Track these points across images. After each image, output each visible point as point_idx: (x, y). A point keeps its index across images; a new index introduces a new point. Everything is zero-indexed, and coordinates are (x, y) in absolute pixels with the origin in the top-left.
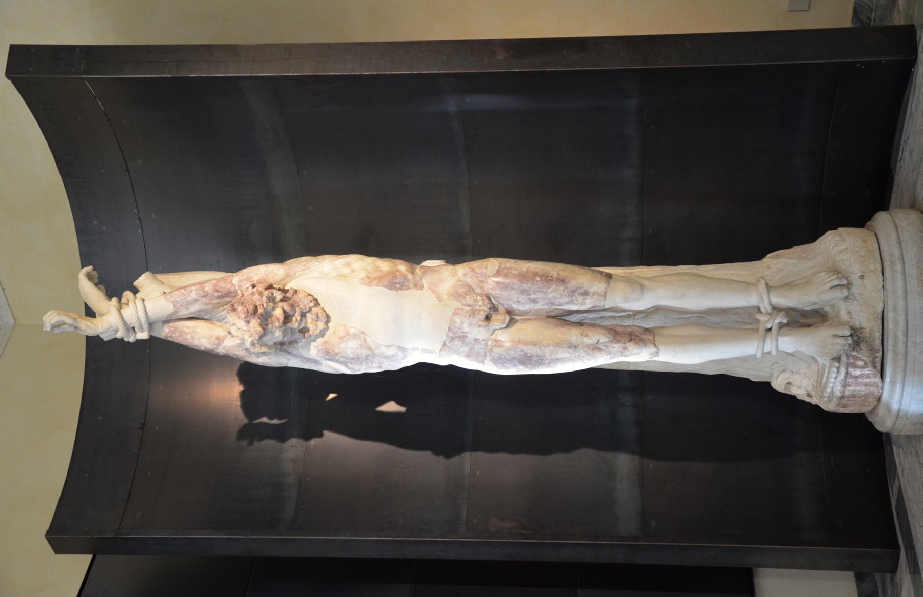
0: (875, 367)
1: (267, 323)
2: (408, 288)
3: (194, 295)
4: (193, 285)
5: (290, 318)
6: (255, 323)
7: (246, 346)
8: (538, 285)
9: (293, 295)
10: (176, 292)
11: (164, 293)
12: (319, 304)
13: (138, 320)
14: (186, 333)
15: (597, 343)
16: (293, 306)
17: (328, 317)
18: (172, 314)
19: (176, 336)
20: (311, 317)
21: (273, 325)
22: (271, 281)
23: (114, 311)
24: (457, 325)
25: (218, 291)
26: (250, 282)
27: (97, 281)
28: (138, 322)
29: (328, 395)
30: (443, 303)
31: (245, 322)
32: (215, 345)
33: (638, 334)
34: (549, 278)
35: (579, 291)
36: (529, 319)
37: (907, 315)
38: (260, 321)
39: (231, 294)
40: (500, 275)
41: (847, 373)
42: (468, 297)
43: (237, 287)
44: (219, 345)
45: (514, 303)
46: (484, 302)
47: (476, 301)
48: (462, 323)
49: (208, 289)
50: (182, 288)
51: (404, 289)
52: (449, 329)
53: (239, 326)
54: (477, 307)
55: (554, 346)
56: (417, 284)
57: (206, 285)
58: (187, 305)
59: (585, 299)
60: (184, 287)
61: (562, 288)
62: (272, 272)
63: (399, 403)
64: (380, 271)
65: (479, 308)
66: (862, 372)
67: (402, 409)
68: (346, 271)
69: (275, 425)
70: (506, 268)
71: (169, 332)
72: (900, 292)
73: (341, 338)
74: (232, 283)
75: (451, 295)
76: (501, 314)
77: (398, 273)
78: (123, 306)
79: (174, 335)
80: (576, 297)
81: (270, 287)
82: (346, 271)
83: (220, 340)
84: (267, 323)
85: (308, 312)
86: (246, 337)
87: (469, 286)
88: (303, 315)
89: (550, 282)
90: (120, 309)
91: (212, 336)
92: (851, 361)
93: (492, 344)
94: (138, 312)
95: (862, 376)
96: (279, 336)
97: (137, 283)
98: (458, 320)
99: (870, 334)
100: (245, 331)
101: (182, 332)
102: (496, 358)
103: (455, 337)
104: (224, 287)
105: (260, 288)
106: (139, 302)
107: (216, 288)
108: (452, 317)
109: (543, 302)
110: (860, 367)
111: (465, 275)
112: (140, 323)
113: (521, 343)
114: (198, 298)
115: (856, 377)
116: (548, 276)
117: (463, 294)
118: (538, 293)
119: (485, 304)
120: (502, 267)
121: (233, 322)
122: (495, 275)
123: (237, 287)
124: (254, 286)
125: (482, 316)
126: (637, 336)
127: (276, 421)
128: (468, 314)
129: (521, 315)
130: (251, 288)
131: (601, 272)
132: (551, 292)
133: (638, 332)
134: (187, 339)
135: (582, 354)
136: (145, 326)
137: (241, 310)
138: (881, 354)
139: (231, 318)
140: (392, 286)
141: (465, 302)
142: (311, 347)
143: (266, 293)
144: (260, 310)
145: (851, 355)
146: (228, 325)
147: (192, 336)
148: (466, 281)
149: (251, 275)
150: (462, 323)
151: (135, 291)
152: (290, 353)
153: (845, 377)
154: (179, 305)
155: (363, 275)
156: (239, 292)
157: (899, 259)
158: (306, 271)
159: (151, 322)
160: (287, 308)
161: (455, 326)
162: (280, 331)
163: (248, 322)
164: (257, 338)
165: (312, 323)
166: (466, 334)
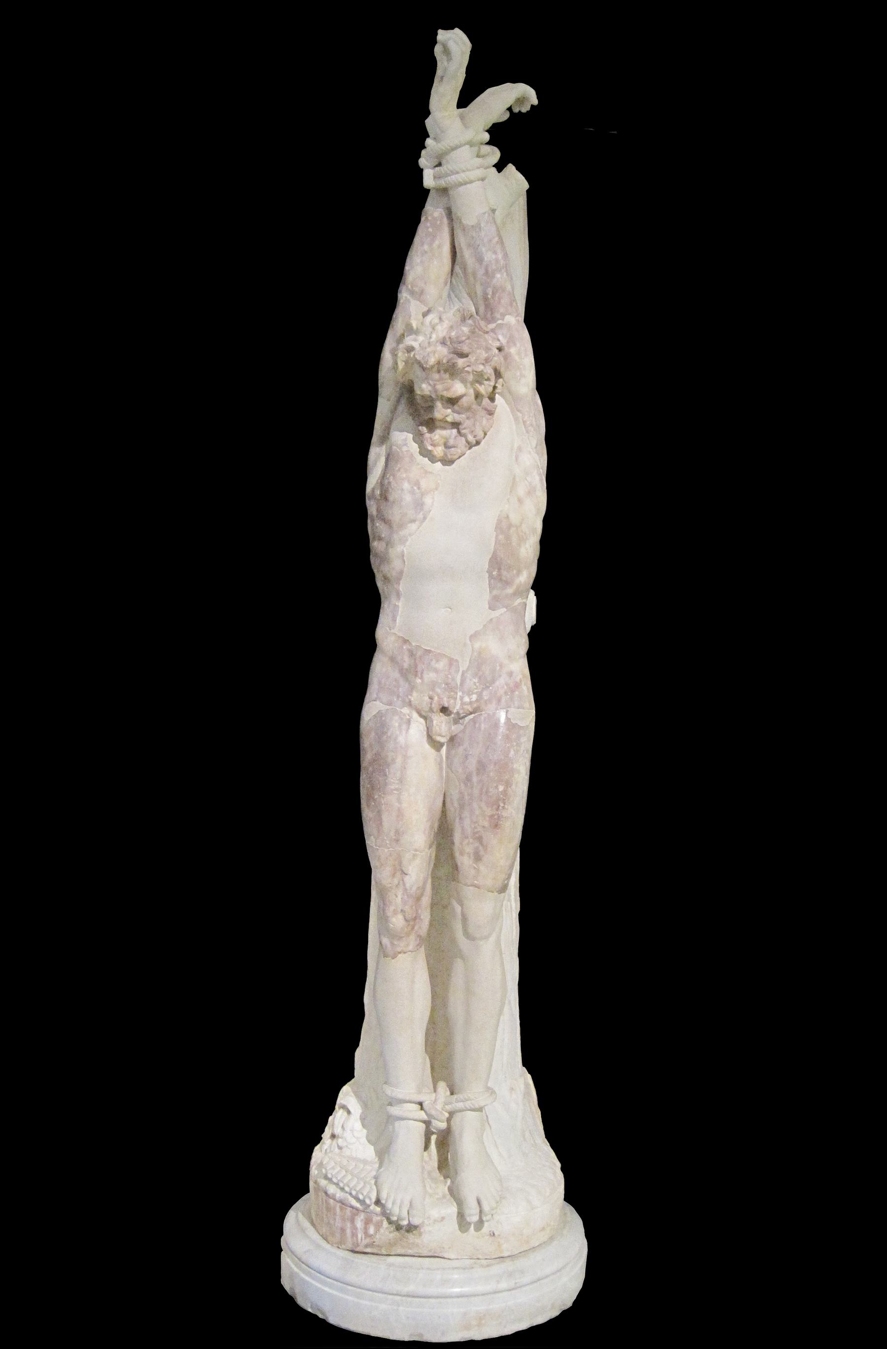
0: (366, 1246)
1: (442, 372)
2: (491, 588)
3: (489, 257)
4: (506, 255)
5: (451, 406)
6: (442, 353)
7: (407, 336)
9: (486, 409)
10: (494, 229)
11: (494, 211)
12: (470, 448)
13: (452, 172)
14: (431, 244)
15: (402, 871)
16: (468, 409)
17: (451, 462)
18: (461, 222)
19: (428, 228)
20: (450, 436)
21: (439, 381)
22: (507, 375)
23: (469, 135)
24: (433, 663)
25: (494, 293)
26: (508, 342)
27: (516, 110)
28: (449, 172)
30: (468, 642)
31: (444, 338)
32: (412, 287)
33: (416, 928)
34: (502, 805)
35: (481, 848)
36: (441, 769)
37: (437, 1297)
38: (444, 361)
39: (489, 313)
40: (508, 729)
42: (476, 680)
43: (500, 322)
44: (412, 293)
45: (465, 750)
46: (467, 704)
47: (470, 693)
48: (436, 671)
50: (500, 237)
53: (439, 328)
54: (460, 694)
56: (497, 601)
57: (505, 274)
58: (472, 246)
60: (501, 242)
62: (522, 376)
64: (519, 545)
65: (458, 697)
68: (521, 491)
70: (519, 737)
73: (417, 484)
74: (507, 314)
75: (480, 653)
76: (450, 728)
77: (515, 572)
78: (476, 149)
79: (428, 224)
81: (498, 374)
82: (521, 491)
83: (419, 295)
84: (442, 372)
85: (459, 432)
86: (421, 338)
87: (493, 681)
88: (456, 425)
90: (471, 144)
91: (425, 283)
93: (404, 715)
94: (464, 171)
95: (354, 1228)
96: (422, 390)
97: (511, 168)
99: (413, 1243)
100: (430, 338)
101: (434, 237)
102: (383, 719)
105: (497, 359)
106: (479, 173)
110: (366, 1229)
111: (510, 674)
112: (447, 175)
114: (484, 263)
115: (352, 1221)
116: (504, 804)
117: (481, 673)
119: (465, 707)
120: (521, 732)
121: (444, 317)
122: (508, 719)
123: (500, 322)
124: (500, 349)
126: (413, 928)
128: (450, 681)
129: (447, 758)
130: (498, 344)
131: (509, 877)
133: (420, 928)
134: (423, 244)
136: (442, 183)
137: (463, 331)
138: (385, 1253)
139: (451, 315)
140: (496, 563)
141: (468, 675)
142: (405, 433)
143: (489, 371)
144: (461, 362)
146: (441, 309)
147: (426, 252)
148: (500, 676)
149: (518, 345)
150: (436, 671)
151: (500, 167)
152: (398, 401)
154: (474, 235)
155: (514, 518)
156: (492, 326)
157: (516, 1283)
158: (523, 427)
159: (451, 192)
160: (464, 401)
161: (432, 660)
162: (430, 391)
163: (443, 343)
164: (418, 357)
165: (442, 437)
166: (420, 675)
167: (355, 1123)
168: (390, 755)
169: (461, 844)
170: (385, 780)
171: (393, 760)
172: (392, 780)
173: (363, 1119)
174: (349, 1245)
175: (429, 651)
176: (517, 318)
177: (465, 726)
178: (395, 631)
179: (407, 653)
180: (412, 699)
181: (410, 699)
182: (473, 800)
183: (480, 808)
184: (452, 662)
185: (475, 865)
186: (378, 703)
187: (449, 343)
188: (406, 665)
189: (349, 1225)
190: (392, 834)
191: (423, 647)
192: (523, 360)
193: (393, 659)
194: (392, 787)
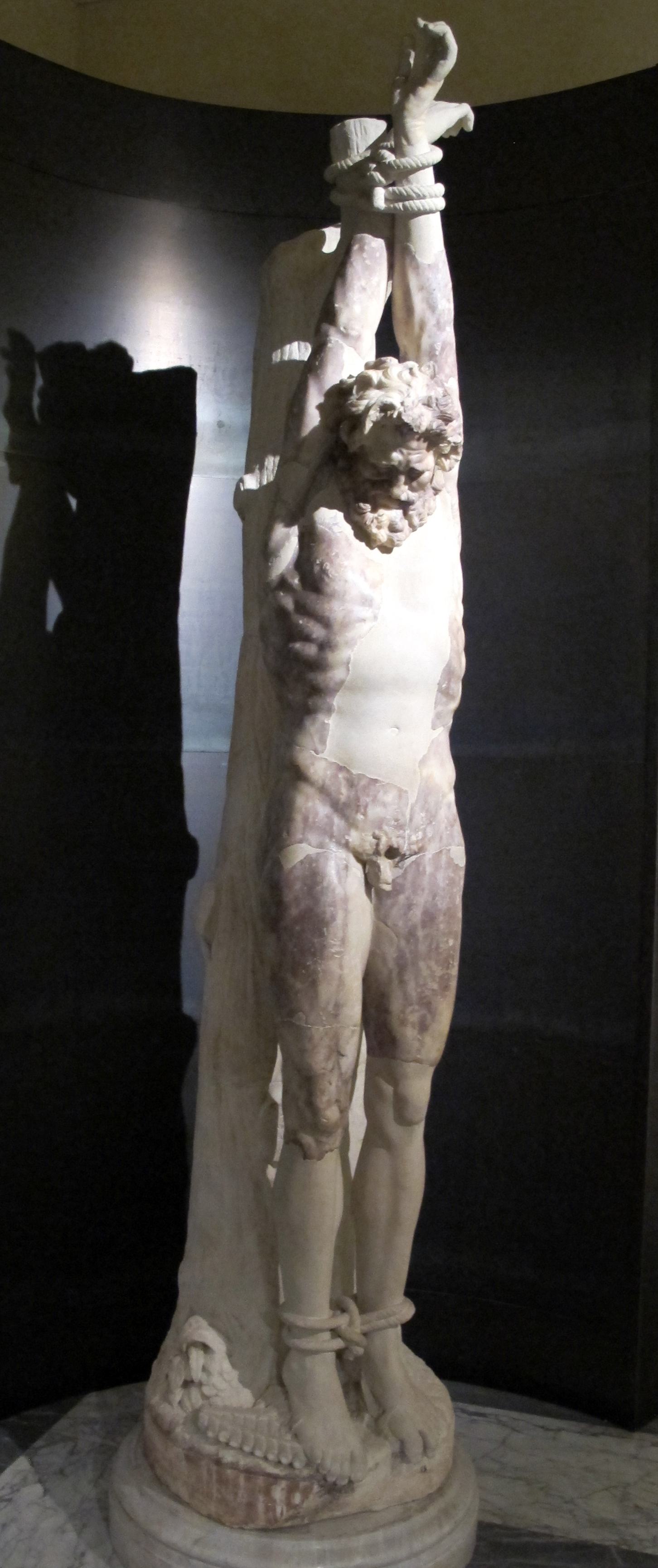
29: (74, 496)
30: (418, 770)
41: (276, 1478)
45: (408, 898)
48: (384, 805)
51: (437, 696)
63: (61, 620)
66: (278, 1501)
67: (50, 626)
69: (30, 399)
72: (417, 1546)
91: (362, 327)
92: (302, 1484)
104: (446, 362)
108: (395, 786)
109: (407, 951)
115: (267, 1492)
127: (36, 401)
141: (417, 809)
145: (312, 1484)
148: (441, 808)
153: (269, 1475)
166: (362, 810)
167: (221, 1362)
168: (329, 910)
169: (403, 1012)
171: (333, 918)
172: (332, 942)
173: (230, 1355)
174: (261, 1522)
175: (376, 781)
177: (406, 870)
178: (324, 755)
180: (350, 840)
181: (347, 840)
183: (429, 967)
184: (401, 793)
185: (419, 1036)
186: (304, 845)
187: (434, 405)
188: (343, 798)
189: (261, 1498)
190: (330, 1008)
191: (369, 776)
193: (323, 790)
194: (333, 950)
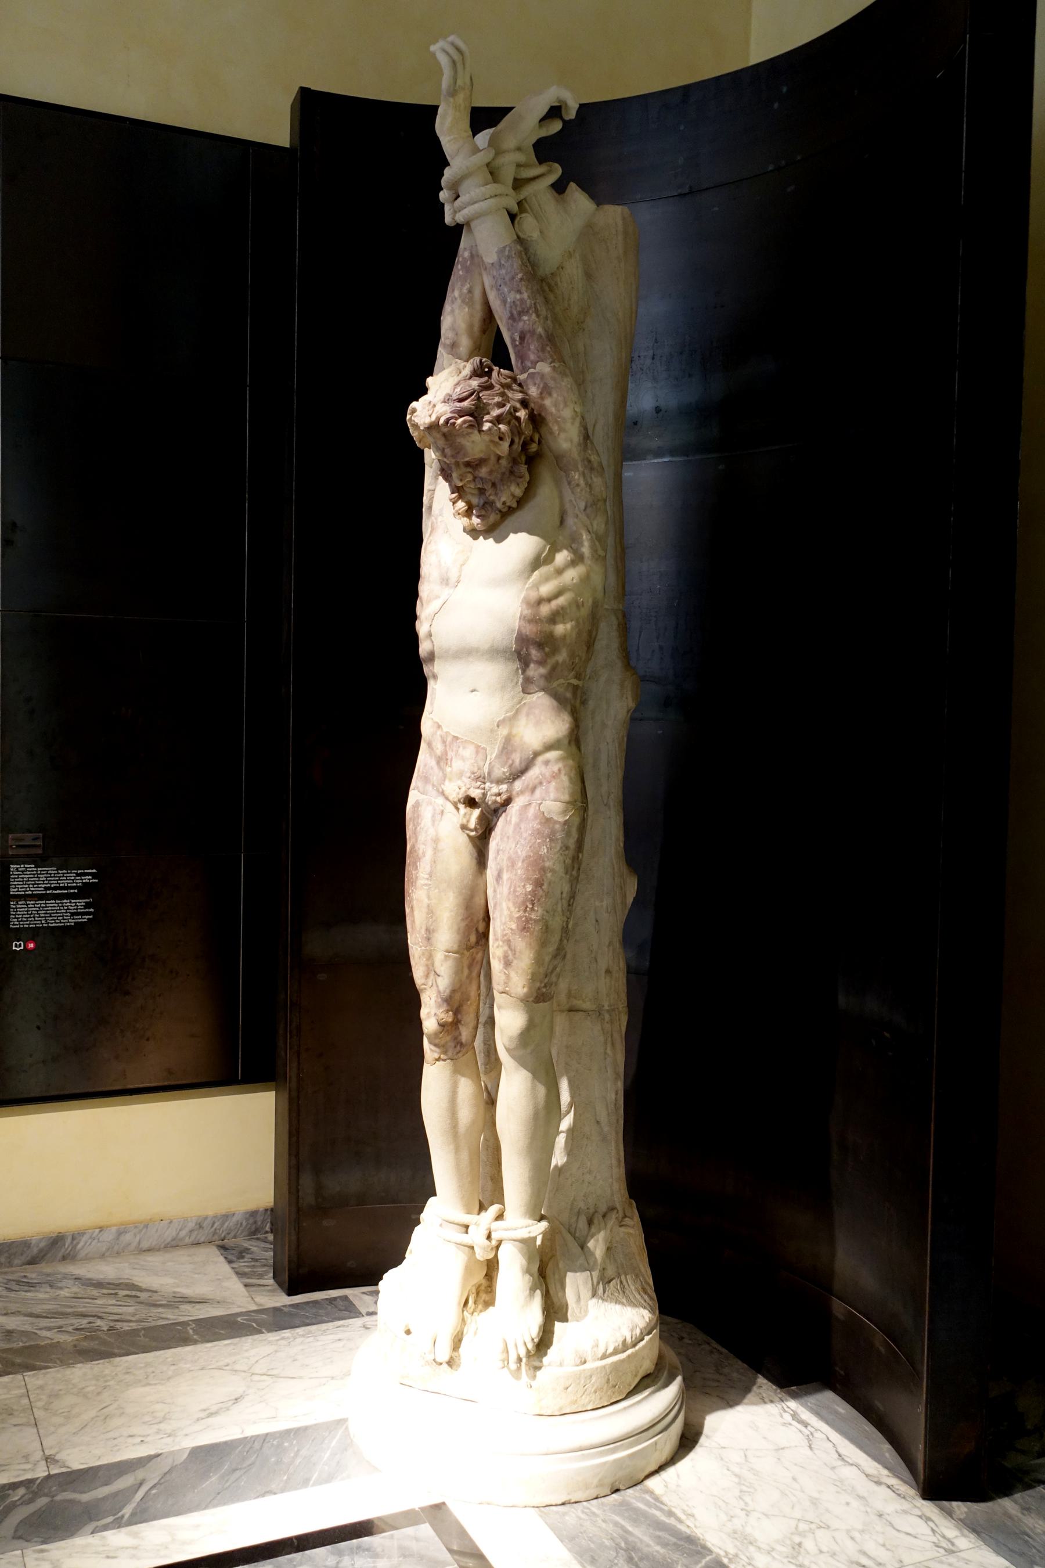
8: (519, 886)
35: (510, 952)
43: (532, 370)
48: (463, 759)
49: (525, 321)
52: (456, 738)
55: (428, 906)
57: (534, 315)
59: (500, 961)
61: (514, 926)
71: (463, 258)
74: (538, 362)
80: (501, 946)
89: (523, 908)
98: (468, 752)
103: (446, 746)
107: (528, 336)
113: (435, 853)
118: (509, 885)
123: (532, 370)
125: (476, 794)
132: (509, 909)
135: (419, 949)
149: (555, 395)
150: (463, 759)
161: (459, 747)
170: (417, 873)
171: (424, 853)
176: (552, 365)
179: (440, 739)
182: (568, 910)
192: (561, 412)
